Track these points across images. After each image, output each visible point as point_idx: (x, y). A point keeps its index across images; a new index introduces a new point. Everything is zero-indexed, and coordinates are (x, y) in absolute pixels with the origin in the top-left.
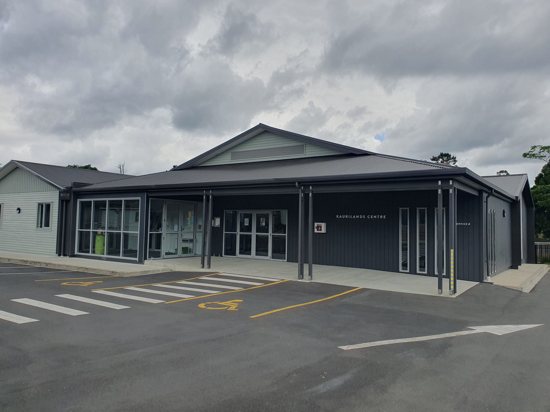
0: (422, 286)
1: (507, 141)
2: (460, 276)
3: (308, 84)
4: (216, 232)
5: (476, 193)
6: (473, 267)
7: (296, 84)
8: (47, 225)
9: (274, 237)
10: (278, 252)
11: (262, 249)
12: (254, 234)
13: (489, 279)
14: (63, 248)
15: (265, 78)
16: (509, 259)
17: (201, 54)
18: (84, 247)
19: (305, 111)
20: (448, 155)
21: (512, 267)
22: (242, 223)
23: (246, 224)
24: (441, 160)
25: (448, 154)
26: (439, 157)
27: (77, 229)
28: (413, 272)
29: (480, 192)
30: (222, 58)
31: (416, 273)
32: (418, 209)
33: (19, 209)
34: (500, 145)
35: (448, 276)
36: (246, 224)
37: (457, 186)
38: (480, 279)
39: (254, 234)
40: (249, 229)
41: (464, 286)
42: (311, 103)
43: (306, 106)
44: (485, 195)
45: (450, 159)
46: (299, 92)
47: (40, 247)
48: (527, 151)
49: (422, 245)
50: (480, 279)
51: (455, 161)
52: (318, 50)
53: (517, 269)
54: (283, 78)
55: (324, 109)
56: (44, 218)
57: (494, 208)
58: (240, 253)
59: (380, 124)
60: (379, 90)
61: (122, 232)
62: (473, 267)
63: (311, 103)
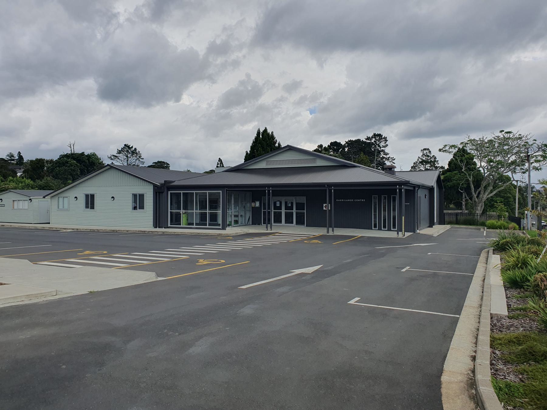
0: (392, 234)
1: (428, 114)
2: (405, 231)
3: (244, 57)
4: (254, 210)
5: (412, 189)
6: (411, 227)
7: (234, 56)
8: (142, 207)
9: (297, 213)
10: (300, 222)
11: (289, 220)
12: (283, 211)
13: (418, 231)
14: (158, 222)
15: (201, 49)
16: (428, 221)
17: (128, 20)
18: (176, 220)
19: (242, 83)
20: (380, 135)
21: (429, 227)
22: (275, 203)
23: (278, 205)
24: (374, 139)
25: (380, 134)
26: (372, 137)
27: (169, 211)
28: (380, 229)
29: (414, 187)
30: (154, 26)
31: (381, 230)
32: (382, 196)
33: (113, 197)
34: (423, 118)
35: (401, 231)
36: (278, 205)
37: (405, 188)
38: (414, 231)
39: (283, 211)
40: (280, 208)
41: (407, 234)
42: (248, 76)
43: (243, 77)
44: (417, 189)
45: (382, 139)
46: (236, 64)
47: (144, 221)
48: (441, 148)
49: (375, 215)
50: (414, 231)
51: (386, 141)
52: (252, 20)
53: (165, 181)
54: (218, 49)
55: (261, 83)
56: (138, 202)
57: (421, 194)
58: (286, 222)
59: (314, 98)
60: (313, 64)
61: (208, 211)
62: (411, 227)
63: (248, 76)
